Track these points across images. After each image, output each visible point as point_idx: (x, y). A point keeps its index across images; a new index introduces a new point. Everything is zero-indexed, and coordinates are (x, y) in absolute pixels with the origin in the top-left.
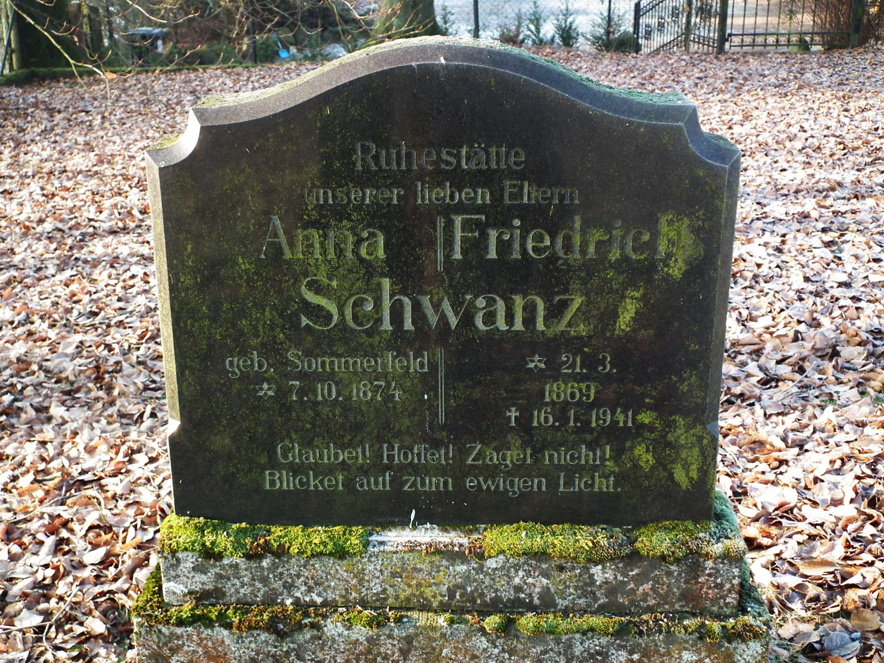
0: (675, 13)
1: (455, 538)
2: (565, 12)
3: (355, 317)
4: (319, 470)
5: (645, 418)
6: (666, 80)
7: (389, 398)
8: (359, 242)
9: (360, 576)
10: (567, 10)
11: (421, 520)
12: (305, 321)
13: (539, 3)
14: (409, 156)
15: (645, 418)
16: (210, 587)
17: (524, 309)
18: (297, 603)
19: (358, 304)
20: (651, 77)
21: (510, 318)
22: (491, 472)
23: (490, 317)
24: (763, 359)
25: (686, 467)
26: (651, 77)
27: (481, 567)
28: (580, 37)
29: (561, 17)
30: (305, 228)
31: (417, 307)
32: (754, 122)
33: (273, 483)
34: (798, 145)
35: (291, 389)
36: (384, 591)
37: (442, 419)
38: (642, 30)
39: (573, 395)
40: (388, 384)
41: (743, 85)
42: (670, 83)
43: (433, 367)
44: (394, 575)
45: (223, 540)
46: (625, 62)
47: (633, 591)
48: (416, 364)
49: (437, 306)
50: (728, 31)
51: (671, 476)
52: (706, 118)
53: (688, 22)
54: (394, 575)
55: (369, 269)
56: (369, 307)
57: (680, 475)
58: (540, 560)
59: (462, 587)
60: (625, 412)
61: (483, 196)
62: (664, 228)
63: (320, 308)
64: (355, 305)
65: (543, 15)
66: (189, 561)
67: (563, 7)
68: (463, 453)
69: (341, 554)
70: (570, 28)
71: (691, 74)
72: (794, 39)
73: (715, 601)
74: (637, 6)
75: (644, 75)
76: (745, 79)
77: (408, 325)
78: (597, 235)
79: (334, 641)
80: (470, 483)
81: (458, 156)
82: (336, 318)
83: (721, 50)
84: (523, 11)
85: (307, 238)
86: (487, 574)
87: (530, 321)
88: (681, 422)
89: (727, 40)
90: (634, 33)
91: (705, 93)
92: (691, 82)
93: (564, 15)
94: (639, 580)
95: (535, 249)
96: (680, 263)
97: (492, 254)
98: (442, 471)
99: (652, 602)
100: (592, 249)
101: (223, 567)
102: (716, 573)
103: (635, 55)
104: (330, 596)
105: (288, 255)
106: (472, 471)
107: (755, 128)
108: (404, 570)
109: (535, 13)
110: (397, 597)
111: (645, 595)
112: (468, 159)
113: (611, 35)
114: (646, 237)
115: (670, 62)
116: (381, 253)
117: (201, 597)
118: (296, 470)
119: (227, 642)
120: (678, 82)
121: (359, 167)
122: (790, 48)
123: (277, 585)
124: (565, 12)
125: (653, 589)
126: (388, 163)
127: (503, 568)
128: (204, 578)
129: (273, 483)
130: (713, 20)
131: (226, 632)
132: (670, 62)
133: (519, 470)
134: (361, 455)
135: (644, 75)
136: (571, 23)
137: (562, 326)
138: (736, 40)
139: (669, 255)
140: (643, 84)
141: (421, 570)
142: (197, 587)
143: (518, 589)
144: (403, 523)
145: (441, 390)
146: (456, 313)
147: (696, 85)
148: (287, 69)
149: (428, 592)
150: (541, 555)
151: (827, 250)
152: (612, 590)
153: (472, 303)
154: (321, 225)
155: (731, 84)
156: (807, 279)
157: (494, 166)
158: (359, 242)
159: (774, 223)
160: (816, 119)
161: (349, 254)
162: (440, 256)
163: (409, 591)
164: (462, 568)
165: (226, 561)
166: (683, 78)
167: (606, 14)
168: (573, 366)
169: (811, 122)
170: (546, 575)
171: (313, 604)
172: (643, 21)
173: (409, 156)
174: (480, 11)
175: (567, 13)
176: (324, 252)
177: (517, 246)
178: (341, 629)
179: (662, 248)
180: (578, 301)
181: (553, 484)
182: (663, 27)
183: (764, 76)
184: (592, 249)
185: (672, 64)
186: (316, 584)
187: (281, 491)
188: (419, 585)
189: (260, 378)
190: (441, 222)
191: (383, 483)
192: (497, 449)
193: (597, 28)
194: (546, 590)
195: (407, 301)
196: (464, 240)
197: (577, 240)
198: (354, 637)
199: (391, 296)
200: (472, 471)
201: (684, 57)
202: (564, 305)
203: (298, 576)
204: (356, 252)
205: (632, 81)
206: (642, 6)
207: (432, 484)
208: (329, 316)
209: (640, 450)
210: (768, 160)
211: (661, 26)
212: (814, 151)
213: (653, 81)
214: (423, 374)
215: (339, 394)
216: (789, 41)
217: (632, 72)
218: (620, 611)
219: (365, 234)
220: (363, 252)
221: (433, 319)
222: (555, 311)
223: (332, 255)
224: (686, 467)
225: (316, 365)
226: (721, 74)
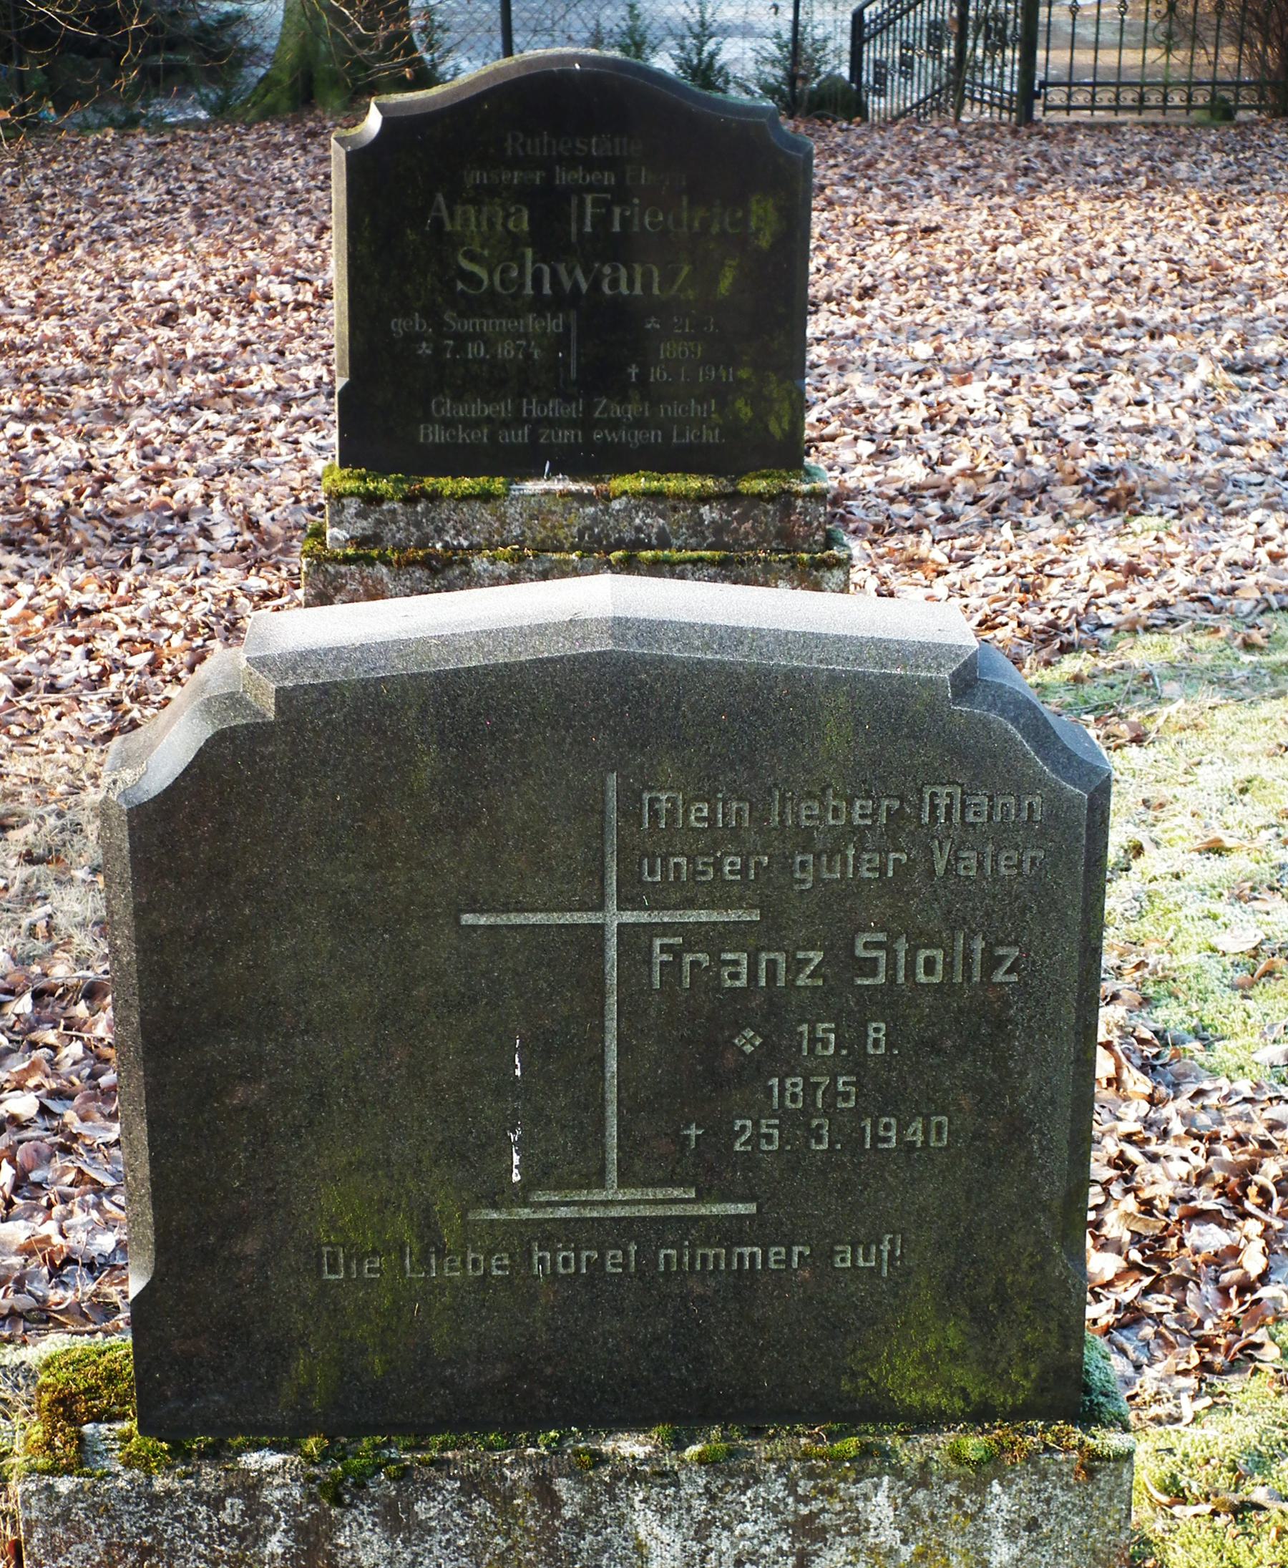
0: (936, 34)
1: (586, 487)
2: (697, 29)
3: (503, 282)
4: (471, 424)
5: (744, 374)
6: (898, 172)
7: (528, 356)
8: (507, 216)
9: (502, 519)
10: (702, 24)
11: (554, 472)
12: (460, 286)
13: (640, 8)
14: (550, 144)
15: (744, 374)
16: (369, 532)
17: (643, 275)
18: (446, 546)
19: (505, 271)
20: (869, 165)
21: (631, 284)
22: (615, 425)
23: (614, 283)
24: (949, 502)
25: (779, 419)
26: (869, 165)
27: (607, 508)
28: (732, 85)
29: (690, 41)
30: (463, 204)
31: (554, 274)
32: (1037, 241)
33: (426, 436)
34: (1102, 274)
35: (446, 347)
36: (523, 533)
37: (573, 375)
38: (867, 76)
39: (683, 353)
40: (529, 345)
41: (1046, 182)
42: (903, 176)
43: (567, 327)
44: (532, 517)
45: (384, 485)
46: (821, 138)
47: (736, 530)
48: (553, 325)
49: (570, 272)
50: (1040, 75)
51: (766, 428)
52: (957, 233)
53: (961, 50)
54: (532, 517)
55: (515, 241)
56: (515, 274)
57: (774, 427)
58: (656, 502)
59: (590, 528)
60: (727, 369)
61: (609, 179)
62: (754, 207)
63: (473, 274)
64: (503, 272)
65: (650, 37)
66: (352, 506)
67: (694, 19)
68: (590, 407)
69: (486, 497)
70: (710, 65)
71: (947, 160)
72: (1201, 98)
73: (805, 538)
74: (858, 16)
75: (855, 162)
76: (1053, 171)
77: (547, 289)
78: (701, 213)
79: (480, 576)
80: (597, 436)
81: (589, 145)
82: (486, 283)
83: (1026, 117)
84: (607, 25)
85: (465, 213)
86: (611, 515)
87: (647, 286)
88: (773, 378)
89: (1038, 96)
90: (852, 80)
91: (968, 195)
92: (946, 175)
93: (696, 36)
94: (742, 519)
95: (651, 224)
96: (768, 237)
97: (617, 228)
98: (571, 424)
99: (752, 540)
100: (696, 224)
101: (382, 513)
102: (805, 512)
103: (845, 125)
104: (476, 539)
105: (448, 228)
106: (599, 424)
107: (1037, 249)
108: (540, 512)
109: (631, 31)
110: (534, 539)
111: (747, 534)
112: (597, 146)
113: (799, 84)
114: (740, 214)
115: (915, 139)
116: (525, 226)
117: (360, 542)
118: (448, 424)
119: (386, 579)
120: (920, 175)
121: (509, 152)
122: (1194, 113)
123: (429, 529)
124: (697, 29)
125: (753, 527)
126: (533, 149)
127: (625, 509)
128: (365, 523)
129: (426, 436)
130: (1008, 53)
131: (384, 570)
132: (915, 139)
133: (640, 423)
134: (504, 409)
135: (855, 162)
136: (712, 55)
137: (673, 291)
138: (1057, 96)
139: (759, 229)
140: (852, 179)
141: (554, 513)
142: (358, 533)
143: (639, 530)
144: (538, 475)
145: (574, 348)
146: (587, 278)
147: (954, 180)
148: (98, 144)
149: (561, 534)
150: (657, 496)
151: (1073, 393)
152: (719, 528)
153: (600, 271)
154: (476, 202)
155: (1021, 180)
156: (1033, 424)
157: (617, 153)
158: (507, 216)
159: (1010, 364)
160: (1151, 235)
161: (499, 228)
162: (574, 228)
163: (544, 533)
164: (591, 510)
165: (385, 507)
166: (932, 168)
167: (787, 35)
168: (683, 327)
169: (1141, 240)
170: (663, 516)
171: (460, 547)
172: (871, 53)
173: (550, 144)
174: (516, 24)
175: (703, 31)
176: (479, 225)
177: (636, 221)
178: (486, 565)
179: (753, 223)
180: (686, 270)
181: (667, 437)
182: (912, 67)
183: (1094, 165)
184: (696, 224)
185: (919, 143)
186: (465, 527)
187: (433, 443)
188: (553, 527)
189: (420, 337)
190: (574, 201)
191: (521, 436)
192: (621, 403)
193: (768, 68)
194: (662, 529)
195: (546, 269)
196: (593, 215)
197: (685, 215)
198: (497, 572)
199: (534, 263)
200: (599, 424)
201: (947, 130)
202: (676, 273)
203: (448, 520)
204: (505, 225)
205: (830, 173)
206: (867, 18)
207: (565, 436)
208: (480, 282)
209: (740, 403)
210: (1043, 295)
211: (906, 62)
212: (1128, 284)
213: (871, 172)
214: (558, 335)
215: (486, 352)
216: (1142, 98)
217: (835, 156)
218: (726, 547)
219: (513, 210)
220: (511, 225)
221: (567, 284)
222: (669, 279)
223: (485, 227)
224: (779, 419)
225: (467, 326)
226: (1008, 160)
